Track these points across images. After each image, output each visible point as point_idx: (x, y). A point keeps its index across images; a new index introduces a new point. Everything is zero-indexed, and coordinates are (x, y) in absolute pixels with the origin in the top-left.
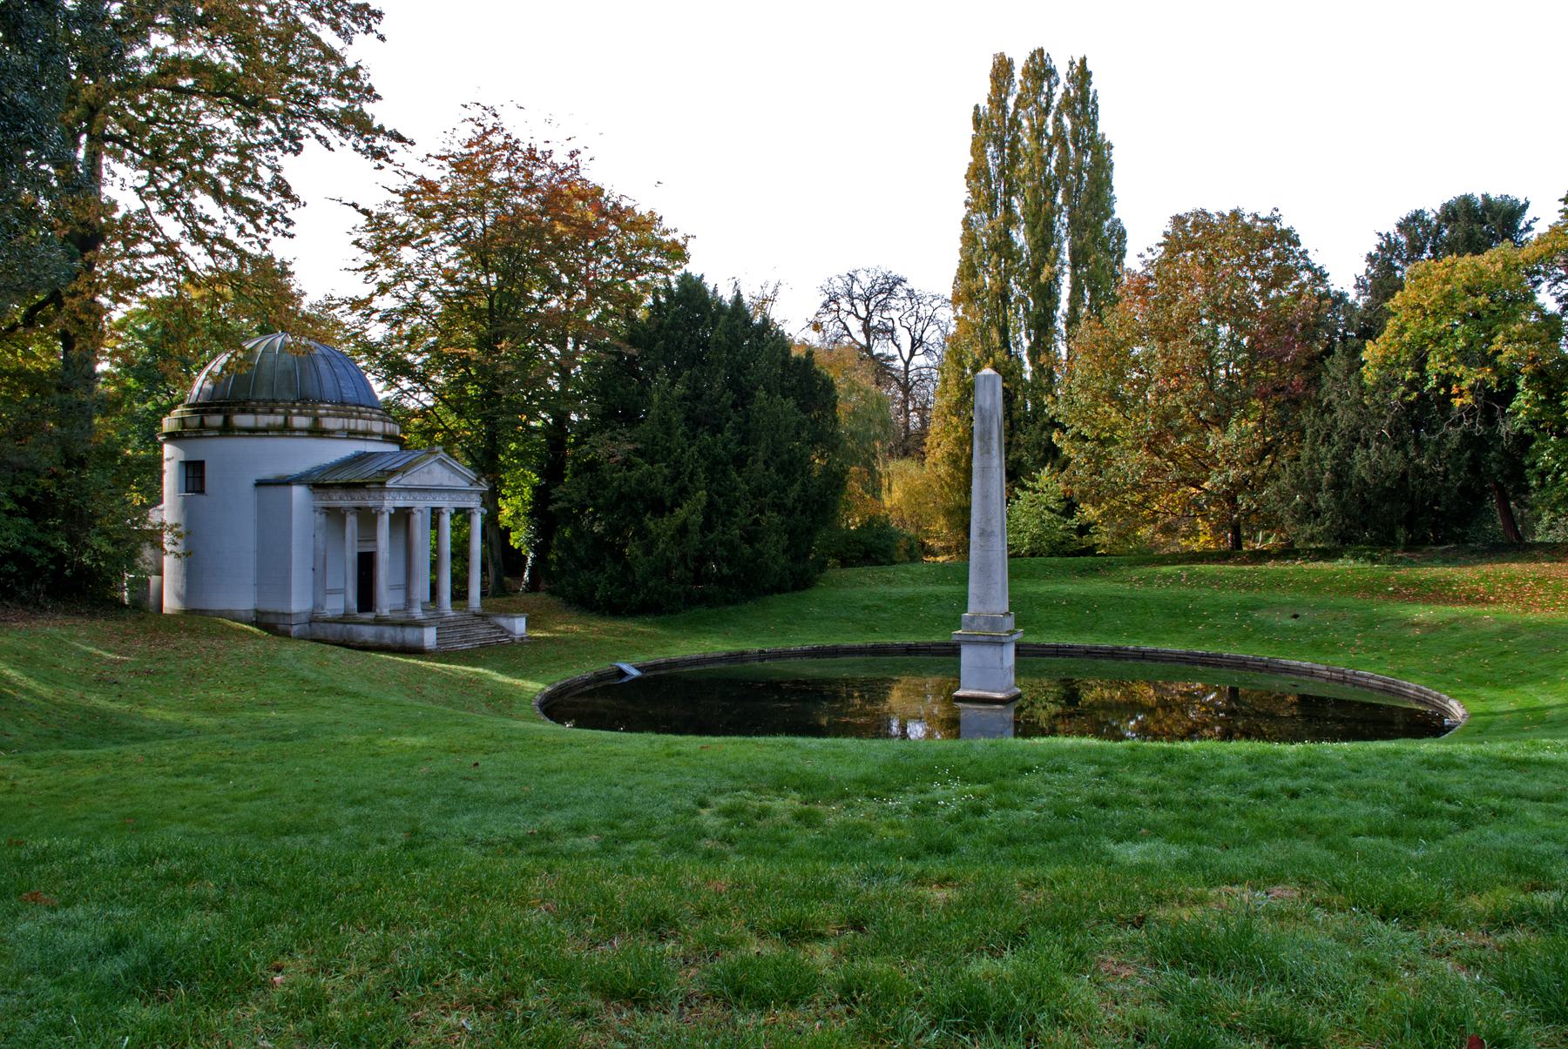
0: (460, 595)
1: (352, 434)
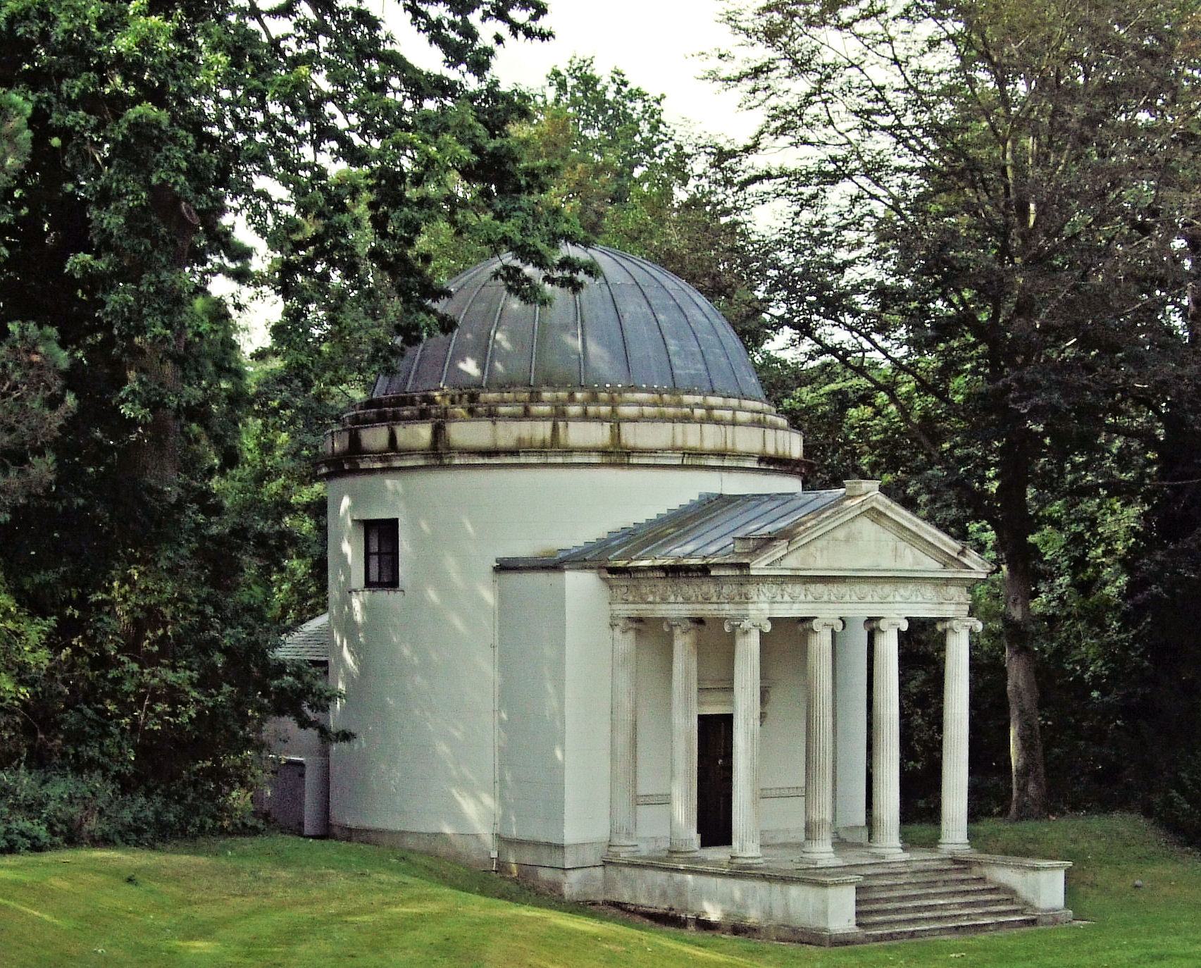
1: (693, 459)
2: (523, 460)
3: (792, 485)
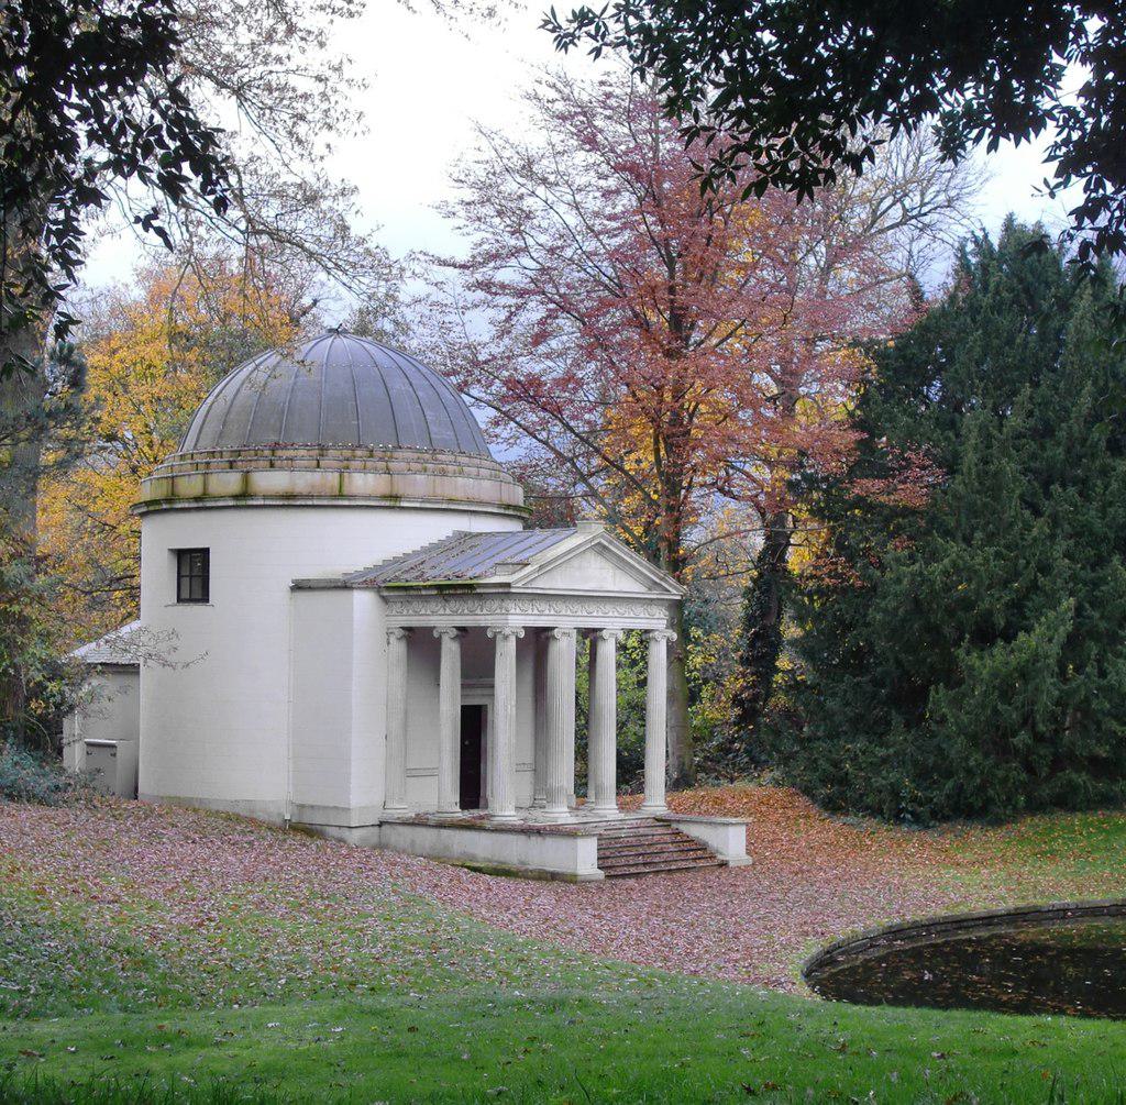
0: (630, 770)
2: (316, 502)
3: (516, 526)
